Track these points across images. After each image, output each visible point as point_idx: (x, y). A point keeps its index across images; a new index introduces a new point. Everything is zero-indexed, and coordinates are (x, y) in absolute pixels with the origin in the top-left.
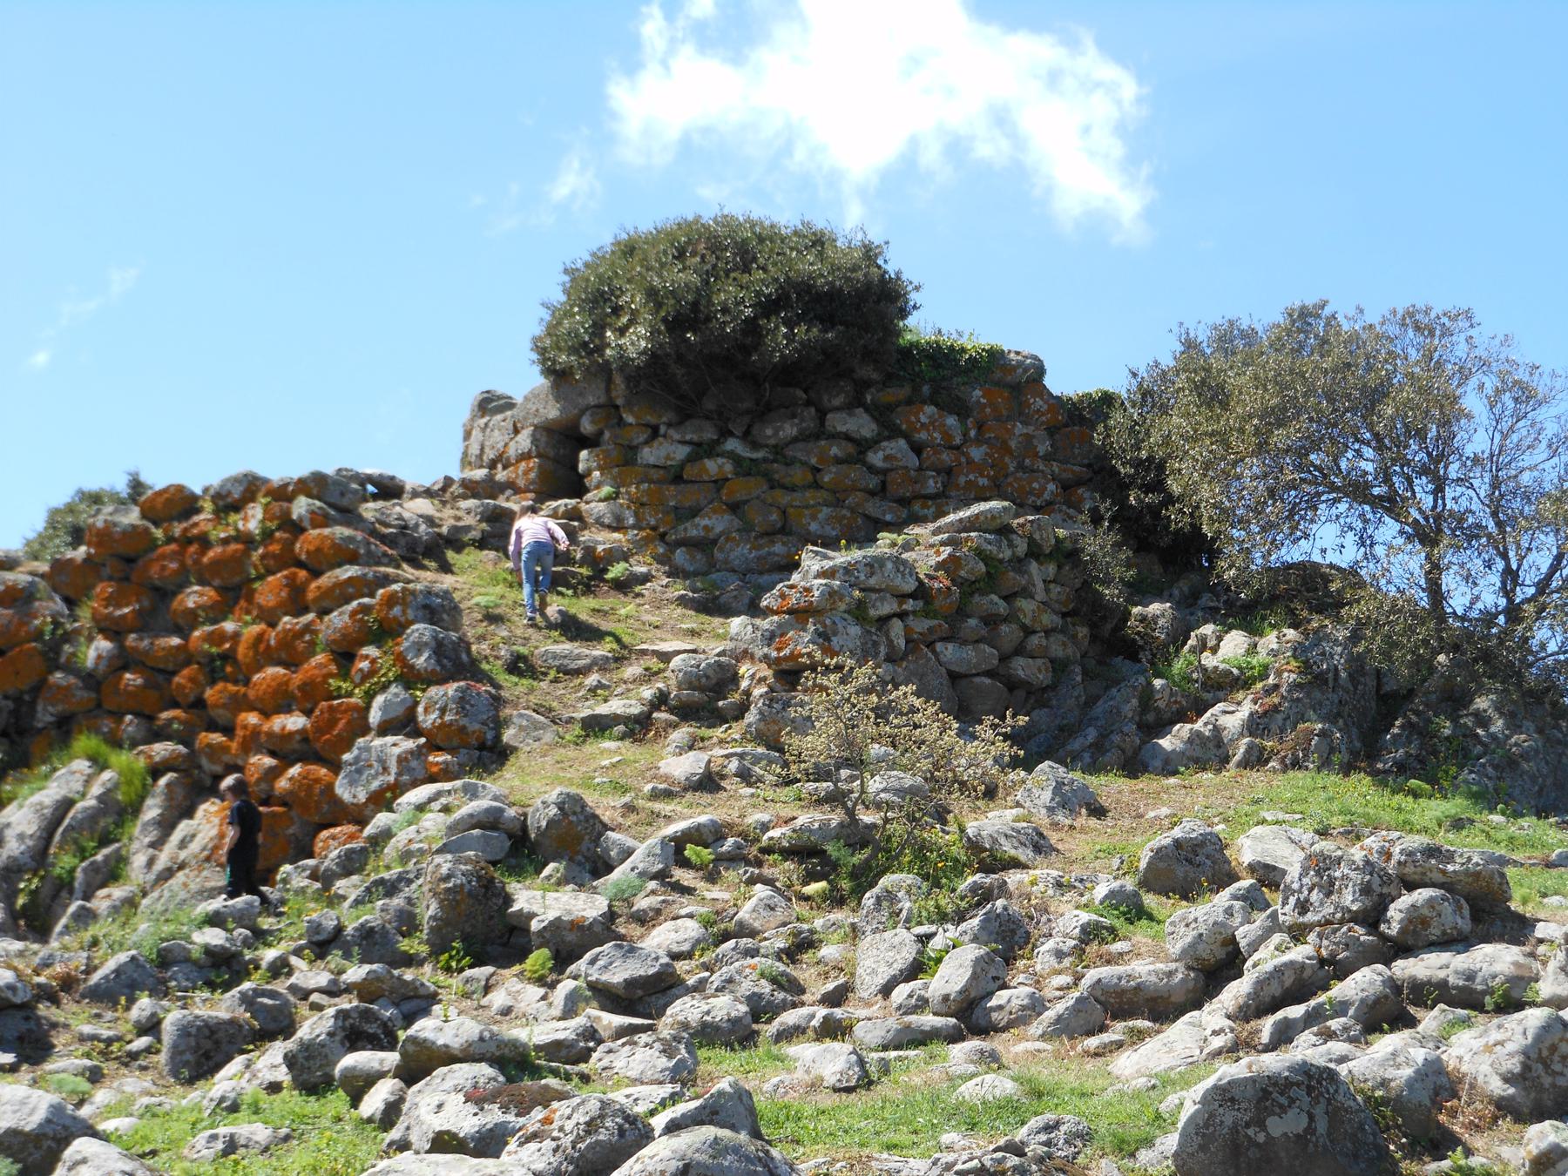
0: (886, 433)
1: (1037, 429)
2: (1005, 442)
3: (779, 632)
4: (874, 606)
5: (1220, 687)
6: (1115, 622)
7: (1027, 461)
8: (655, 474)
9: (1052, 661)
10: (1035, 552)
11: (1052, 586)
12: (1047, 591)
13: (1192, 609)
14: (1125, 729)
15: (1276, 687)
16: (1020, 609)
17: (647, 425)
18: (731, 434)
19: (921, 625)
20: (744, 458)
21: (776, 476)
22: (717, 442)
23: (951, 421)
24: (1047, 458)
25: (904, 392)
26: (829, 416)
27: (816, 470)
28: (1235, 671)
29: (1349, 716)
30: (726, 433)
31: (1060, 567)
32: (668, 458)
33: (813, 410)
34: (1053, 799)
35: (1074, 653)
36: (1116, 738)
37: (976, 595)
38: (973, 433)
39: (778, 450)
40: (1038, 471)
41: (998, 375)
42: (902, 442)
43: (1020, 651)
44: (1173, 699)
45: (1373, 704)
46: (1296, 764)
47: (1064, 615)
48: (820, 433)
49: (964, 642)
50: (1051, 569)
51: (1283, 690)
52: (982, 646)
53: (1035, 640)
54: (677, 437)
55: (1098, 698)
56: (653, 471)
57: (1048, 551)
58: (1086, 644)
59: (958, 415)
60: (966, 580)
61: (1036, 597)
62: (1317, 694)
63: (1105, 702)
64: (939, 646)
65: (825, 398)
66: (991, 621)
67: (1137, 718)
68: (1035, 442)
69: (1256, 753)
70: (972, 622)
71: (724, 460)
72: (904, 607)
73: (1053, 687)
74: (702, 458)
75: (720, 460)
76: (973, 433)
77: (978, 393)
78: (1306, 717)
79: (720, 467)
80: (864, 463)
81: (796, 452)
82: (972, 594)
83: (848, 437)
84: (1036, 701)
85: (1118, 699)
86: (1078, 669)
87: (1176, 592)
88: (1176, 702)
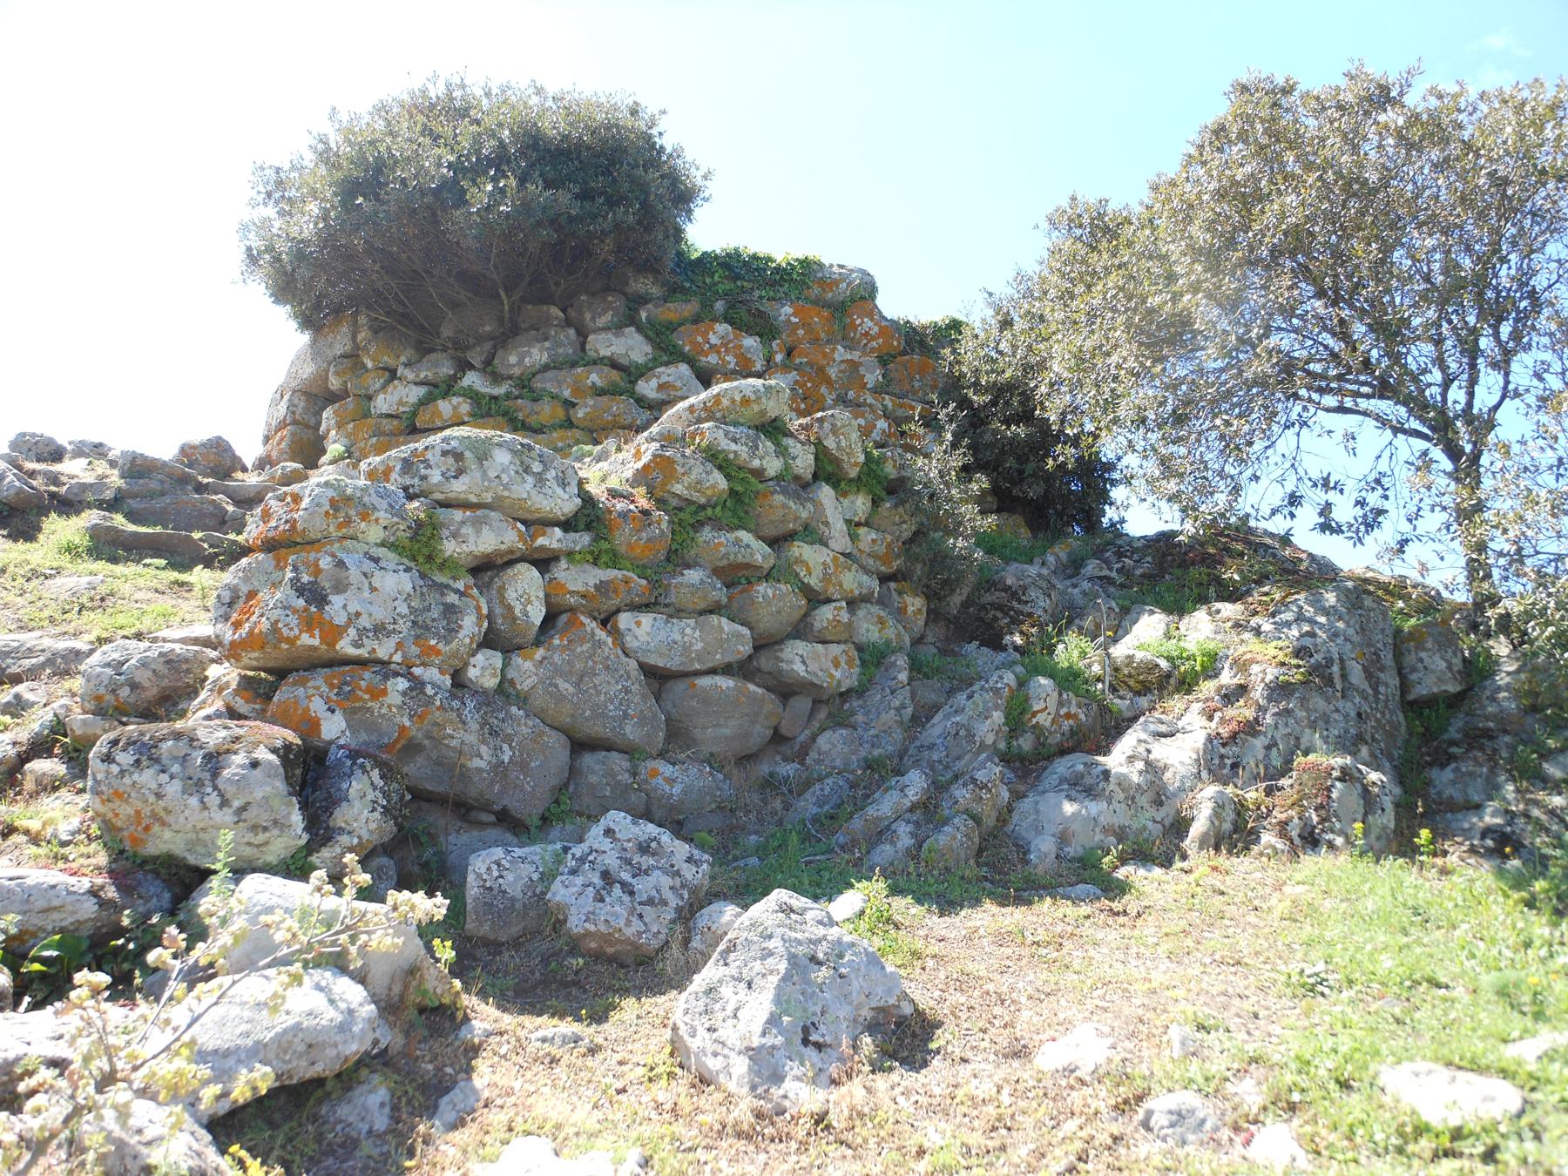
0: (665, 358)
1: (864, 354)
2: (821, 370)
3: (244, 589)
4: (455, 535)
5: (1144, 689)
6: (966, 591)
7: (851, 394)
8: (388, 425)
9: (860, 648)
10: (828, 470)
11: (862, 531)
12: (853, 537)
13: (1074, 580)
14: (981, 776)
15: (1242, 689)
16: (800, 561)
17: (384, 369)
18: (472, 367)
19: (577, 579)
20: (484, 396)
21: (520, 416)
22: (454, 379)
23: (750, 342)
24: (877, 391)
25: (689, 308)
26: (591, 338)
27: (569, 405)
28: (1164, 664)
29: (1373, 739)
30: (464, 366)
31: (875, 503)
32: (400, 403)
33: (572, 332)
34: (773, 1021)
35: (898, 635)
36: (962, 794)
37: (707, 529)
38: (779, 358)
39: (525, 384)
40: (865, 404)
41: (816, 290)
42: (684, 368)
43: (800, 630)
44: (1063, 711)
45: (1401, 717)
46: (1311, 840)
47: (884, 579)
48: (581, 358)
49: (678, 613)
50: (860, 504)
51: (1258, 693)
52: (714, 619)
53: (825, 614)
54: (411, 376)
55: (936, 708)
56: (385, 421)
57: (853, 473)
58: (921, 623)
59: (761, 336)
60: (689, 502)
61: (832, 543)
62: (1318, 702)
63: (947, 717)
64: (624, 620)
65: (588, 316)
66: (736, 576)
67: (1002, 745)
68: (862, 371)
69: (1230, 815)
70: (693, 576)
71: (460, 399)
72: (540, 541)
73: (859, 692)
74: (435, 400)
75: (455, 400)
76: (779, 358)
77: (788, 310)
78: (1304, 743)
79: (455, 408)
80: (632, 394)
81: (545, 383)
82: (698, 526)
83: (614, 364)
84: (830, 715)
85: (969, 712)
86: (902, 661)
87: (1051, 559)
88: (1068, 716)
